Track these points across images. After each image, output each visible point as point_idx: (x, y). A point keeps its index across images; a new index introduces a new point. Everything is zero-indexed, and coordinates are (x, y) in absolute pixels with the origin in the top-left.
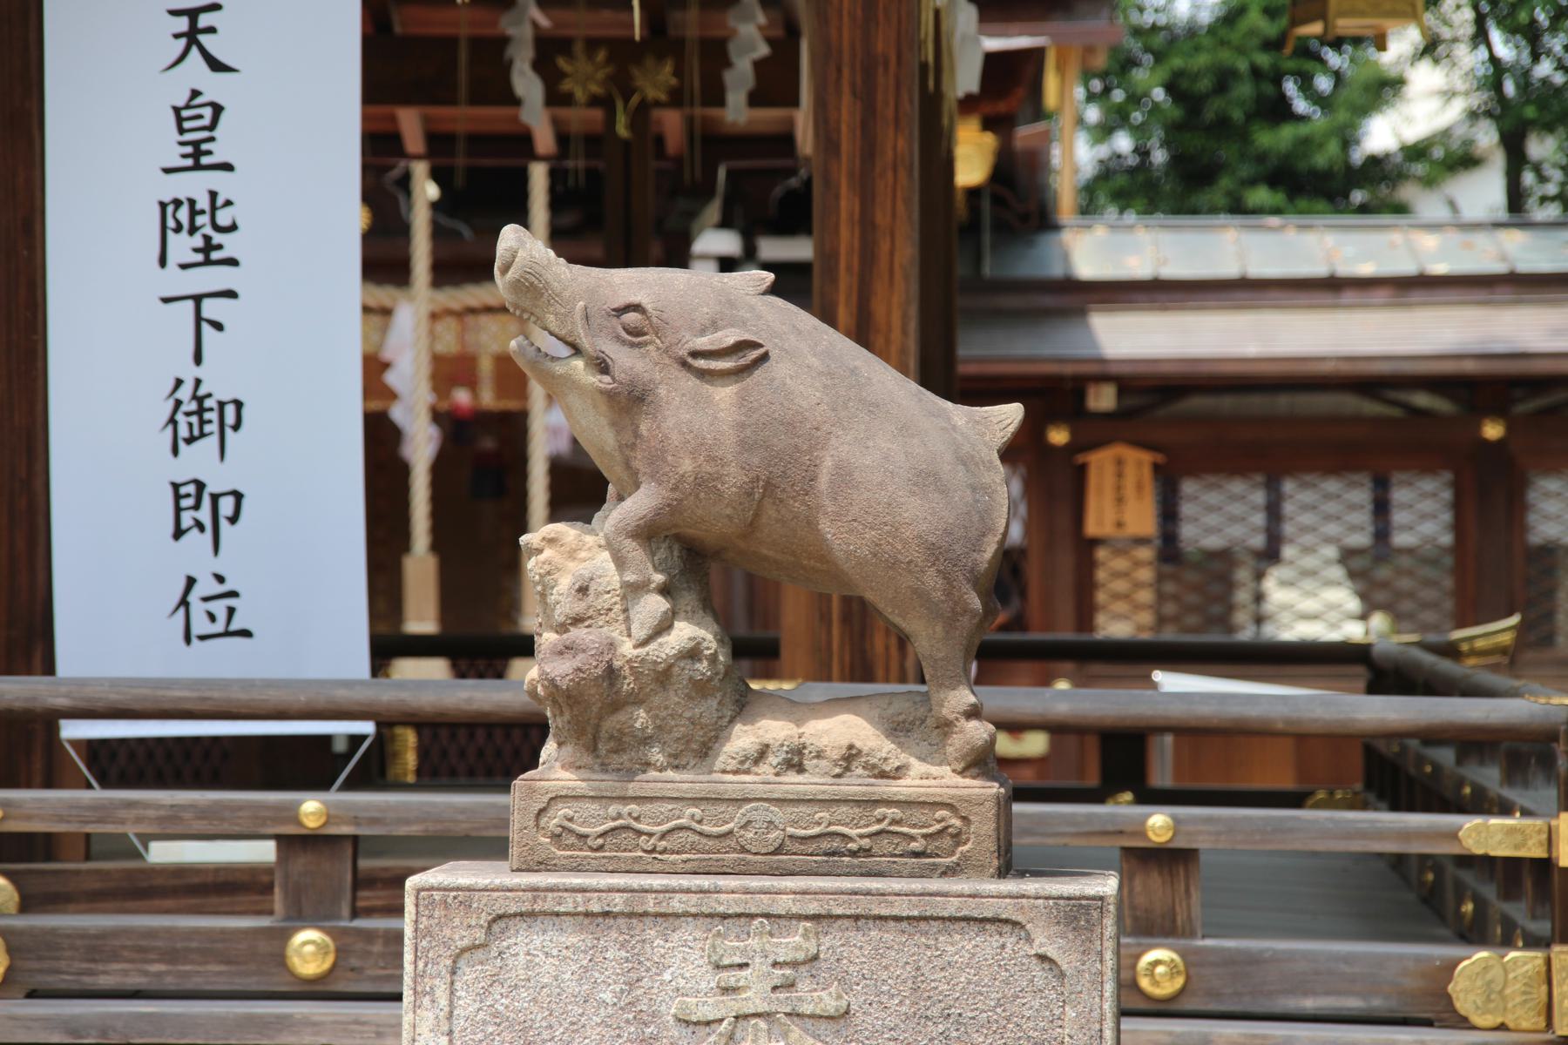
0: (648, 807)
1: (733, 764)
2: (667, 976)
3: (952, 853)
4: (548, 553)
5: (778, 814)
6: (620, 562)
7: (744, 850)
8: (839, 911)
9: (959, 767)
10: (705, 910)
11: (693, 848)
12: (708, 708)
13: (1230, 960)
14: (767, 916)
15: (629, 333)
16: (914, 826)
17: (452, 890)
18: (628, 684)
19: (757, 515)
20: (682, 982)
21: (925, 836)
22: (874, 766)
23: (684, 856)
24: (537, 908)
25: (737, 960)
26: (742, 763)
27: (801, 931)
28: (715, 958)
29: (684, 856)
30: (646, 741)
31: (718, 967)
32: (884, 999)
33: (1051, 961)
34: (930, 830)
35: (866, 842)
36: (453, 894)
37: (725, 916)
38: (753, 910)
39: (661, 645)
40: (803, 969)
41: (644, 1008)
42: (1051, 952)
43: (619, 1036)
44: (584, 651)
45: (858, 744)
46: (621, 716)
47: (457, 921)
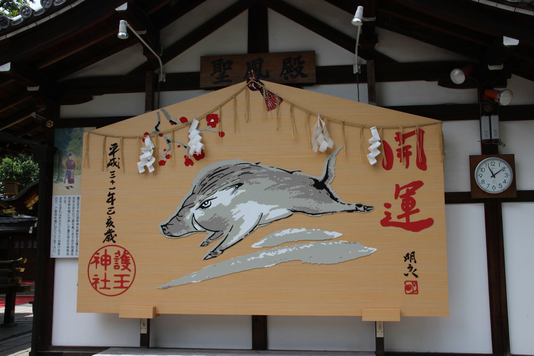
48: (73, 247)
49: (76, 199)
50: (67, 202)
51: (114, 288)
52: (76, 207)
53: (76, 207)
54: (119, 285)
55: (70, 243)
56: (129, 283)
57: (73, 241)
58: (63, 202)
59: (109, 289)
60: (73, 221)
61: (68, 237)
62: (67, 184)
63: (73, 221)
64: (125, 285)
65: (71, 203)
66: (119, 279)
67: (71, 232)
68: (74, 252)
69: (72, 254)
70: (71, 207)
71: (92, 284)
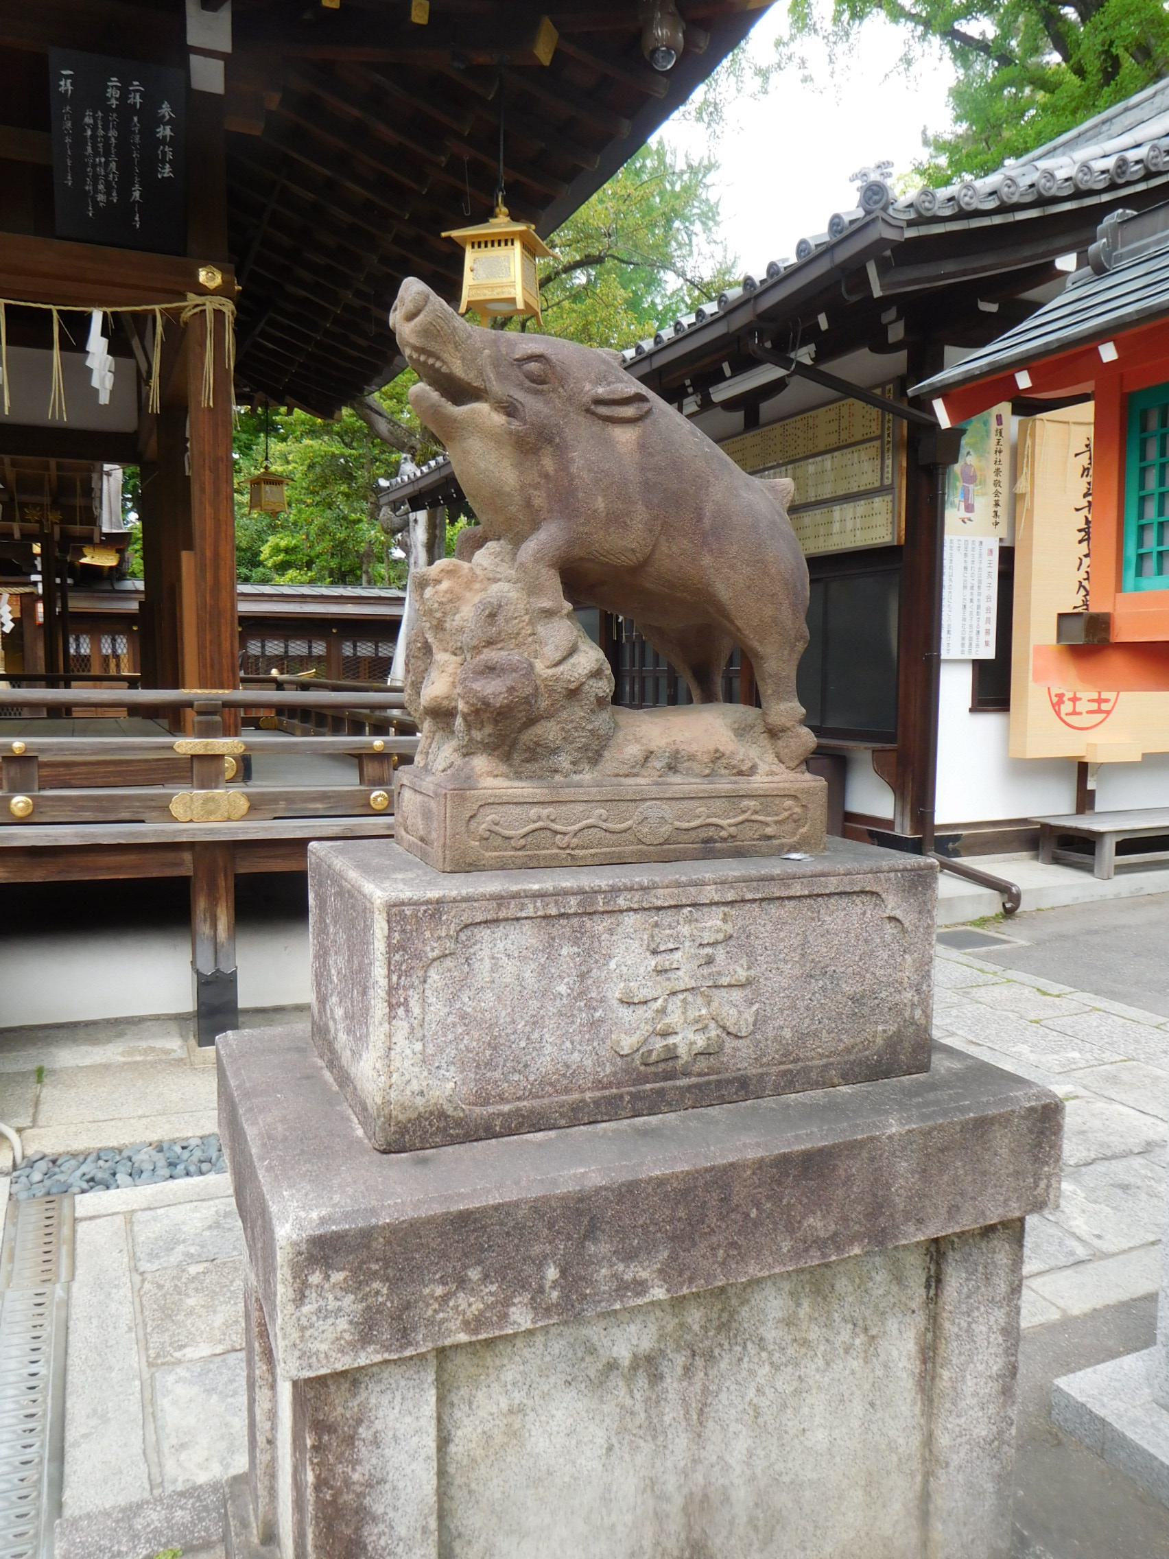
0: (563, 808)
1: (625, 769)
2: (612, 965)
3: (794, 834)
5: (667, 810)
6: (533, 590)
7: (640, 842)
8: (749, 896)
9: (793, 765)
10: (646, 905)
11: (600, 844)
12: (602, 720)
14: (693, 905)
15: (533, 381)
16: (768, 815)
17: (422, 904)
18: (544, 703)
19: (653, 552)
20: (624, 969)
21: (776, 822)
22: (734, 767)
23: (592, 851)
24: (502, 915)
25: (671, 946)
26: (633, 767)
27: (721, 916)
28: (653, 946)
29: (592, 851)
30: (555, 751)
31: (655, 952)
32: (781, 965)
33: (898, 920)
34: (780, 818)
35: (733, 830)
36: (424, 908)
37: (659, 909)
38: (684, 901)
39: (573, 665)
40: (719, 947)
41: (594, 995)
42: (898, 913)
43: (573, 1022)
44: (515, 671)
45: (721, 749)
46: (538, 729)
47: (428, 934)
48: (971, 639)
49: (977, 544)
50: (962, 548)
51: (1088, 712)
52: (977, 560)
53: (977, 560)
54: (1094, 706)
55: (968, 629)
56: (1111, 704)
57: (971, 626)
58: (955, 548)
59: (1080, 714)
60: (972, 588)
61: (964, 619)
62: (963, 513)
63: (972, 588)
64: (1105, 707)
65: (970, 553)
67: (968, 609)
68: (974, 649)
69: (970, 652)
70: (969, 559)
71: (1053, 706)
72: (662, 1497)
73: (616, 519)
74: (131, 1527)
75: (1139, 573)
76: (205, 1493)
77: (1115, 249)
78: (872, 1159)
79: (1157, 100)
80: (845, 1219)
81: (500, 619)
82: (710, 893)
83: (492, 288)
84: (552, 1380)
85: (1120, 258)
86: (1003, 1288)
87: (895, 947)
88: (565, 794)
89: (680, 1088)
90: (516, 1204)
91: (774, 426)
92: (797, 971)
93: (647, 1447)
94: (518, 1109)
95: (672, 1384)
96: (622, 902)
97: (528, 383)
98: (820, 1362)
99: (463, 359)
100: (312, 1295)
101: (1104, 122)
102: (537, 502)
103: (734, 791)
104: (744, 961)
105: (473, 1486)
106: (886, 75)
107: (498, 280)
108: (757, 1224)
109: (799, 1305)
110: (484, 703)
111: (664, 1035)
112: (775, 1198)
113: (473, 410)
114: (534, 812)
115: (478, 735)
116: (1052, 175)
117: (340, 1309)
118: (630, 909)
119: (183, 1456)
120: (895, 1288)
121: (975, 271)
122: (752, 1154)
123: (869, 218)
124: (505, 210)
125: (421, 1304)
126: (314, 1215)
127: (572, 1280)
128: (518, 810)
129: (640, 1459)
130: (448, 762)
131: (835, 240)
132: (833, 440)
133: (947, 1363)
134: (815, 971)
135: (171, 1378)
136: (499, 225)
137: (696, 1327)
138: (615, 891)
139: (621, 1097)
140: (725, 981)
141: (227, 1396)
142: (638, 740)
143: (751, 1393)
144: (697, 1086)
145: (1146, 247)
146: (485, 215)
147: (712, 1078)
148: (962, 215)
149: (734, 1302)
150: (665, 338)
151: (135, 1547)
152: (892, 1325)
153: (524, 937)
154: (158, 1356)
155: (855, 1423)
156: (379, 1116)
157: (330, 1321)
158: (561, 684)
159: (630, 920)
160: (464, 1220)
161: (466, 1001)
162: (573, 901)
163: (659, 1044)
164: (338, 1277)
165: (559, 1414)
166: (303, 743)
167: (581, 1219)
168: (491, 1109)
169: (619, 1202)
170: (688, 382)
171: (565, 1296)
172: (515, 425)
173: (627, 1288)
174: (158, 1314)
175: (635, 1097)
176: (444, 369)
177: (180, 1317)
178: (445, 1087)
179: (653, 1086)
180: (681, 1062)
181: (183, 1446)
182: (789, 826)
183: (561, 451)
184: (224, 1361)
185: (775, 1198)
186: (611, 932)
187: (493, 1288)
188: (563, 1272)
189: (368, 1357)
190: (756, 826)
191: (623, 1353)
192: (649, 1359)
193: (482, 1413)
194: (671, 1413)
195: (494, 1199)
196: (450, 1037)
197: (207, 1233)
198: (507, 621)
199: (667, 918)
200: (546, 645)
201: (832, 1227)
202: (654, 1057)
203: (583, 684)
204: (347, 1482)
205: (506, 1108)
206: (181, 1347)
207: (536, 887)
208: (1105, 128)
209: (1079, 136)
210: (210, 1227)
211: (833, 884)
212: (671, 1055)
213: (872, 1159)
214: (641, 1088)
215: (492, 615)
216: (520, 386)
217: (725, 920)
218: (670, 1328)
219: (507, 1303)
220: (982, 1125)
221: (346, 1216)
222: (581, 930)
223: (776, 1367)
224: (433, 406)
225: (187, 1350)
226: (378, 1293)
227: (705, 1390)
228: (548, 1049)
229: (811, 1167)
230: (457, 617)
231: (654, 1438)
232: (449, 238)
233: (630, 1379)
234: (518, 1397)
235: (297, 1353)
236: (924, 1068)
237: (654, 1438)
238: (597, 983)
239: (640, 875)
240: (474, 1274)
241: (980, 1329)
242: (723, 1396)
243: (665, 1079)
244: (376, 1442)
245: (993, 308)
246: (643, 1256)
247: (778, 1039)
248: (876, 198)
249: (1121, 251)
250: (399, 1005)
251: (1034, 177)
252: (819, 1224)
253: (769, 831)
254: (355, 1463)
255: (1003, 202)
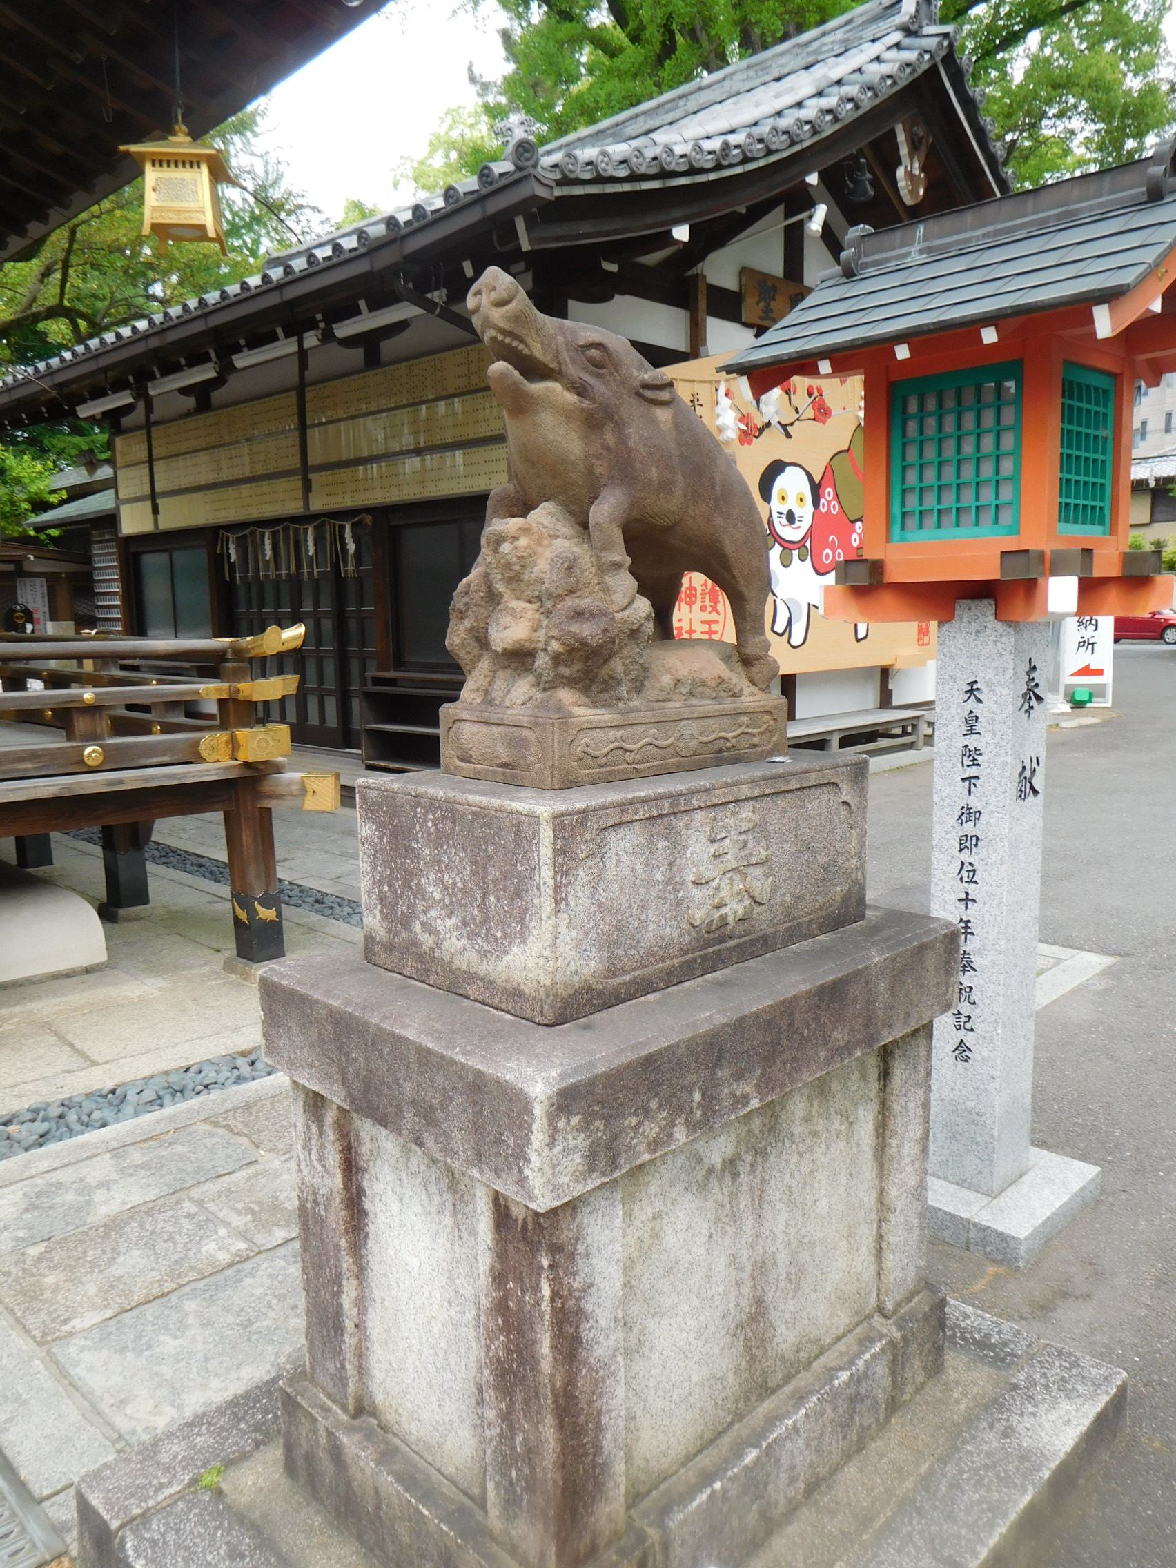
1: (663, 695)
4: (523, 542)
8: (767, 792)
10: (709, 803)
13: (118, 747)
21: (761, 733)
23: (649, 764)
29: (649, 764)
31: (713, 841)
37: (715, 806)
47: (579, 839)
66: (706, 628)
72: (740, 1269)
73: (665, 487)
74: (158, 1463)
75: (903, 528)
76: (213, 1418)
77: (860, 258)
78: (867, 983)
79: (727, 83)
80: (853, 1031)
81: (577, 571)
82: (746, 791)
83: (179, 212)
84: (677, 1188)
85: (865, 266)
86: (923, 1074)
87: (846, 825)
88: (632, 718)
89: (728, 949)
90: (678, 1045)
91: (398, 366)
92: (793, 849)
93: (731, 1230)
94: (635, 978)
95: (744, 1179)
96: (695, 803)
97: (591, 368)
98: (823, 1147)
99: (542, 343)
100: (559, 1137)
101: (681, 97)
102: (598, 470)
103: (735, 709)
104: (764, 843)
105: (633, 1282)
106: (454, 12)
107: (184, 205)
108: (807, 1040)
109: (812, 1105)
110: (581, 644)
111: (717, 907)
112: (816, 1019)
113: (548, 389)
114: (612, 733)
115: (566, 671)
116: (671, 150)
117: (576, 1147)
118: (700, 808)
119: (129, 1410)
120: (862, 1084)
121: (598, 235)
122: (805, 987)
123: (519, 175)
124: (184, 128)
125: (623, 1135)
126: (554, 1073)
127: (709, 1100)
128: (600, 733)
129: (727, 1241)
130: (527, 696)
131: (485, 191)
132: (462, 384)
133: (894, 1133)
134: (804, 848)
135: (72, 1350)
136: (180, 145)
137: (757, 1132)
138: (691, 793)
139: (695, 960)
140: (754, 860)
141: (142, 1351)
142: (668, 671)
143: (787, 1177)
144: (739, 946)
145: (887, 260)
146: (166, 130)
147: (747, 938)
148: (600, 179)
149: (778, 1108)
150: (296, 269)
151: (174, 1476)
152: (861, 1112)
153: (632, 838)
154: (44, 1335)
155: (843, 1189)
156: (547, 997)
157: (570, 1158)
158: (627, 625)
159: (699, 816)
160: (649, 1063)
161: (602, 895)
162: (666, 803)
163: (716, 915)
164: (575, 1120)
165: (681, 1215)
166: (107, 693)
167: (713, 1050)
168: (618, 980)
169: (735, 1034)
170: (319, 317)
171: (704, 1114)
172: (586, 404)
173: (738, 1102)
174: (20, 1298)
175: (704, 958)
176: (526, 351)
177: (48, 1295)
178: (584, 965)
179: (716, 949)
180: (729, 927)
181: (122, 1403)
182: (765, 737)
183: (619, 427)
184: (119, 1322)
185: (816, 1019)
186: (687, 827)
187: (664, 1114)
188: (703, 1095)
189: (594, 1182)
190: (747, 737)
191: (716, 1159)
192: (732, 1161)
193: (637, 1222)
194: (744, 1201)
195: (664, 1043)
196: (592, 924)
197: (27, 1216)
198: (582, 573)
199: (719, 813)
200: (615, 592)
201: (846, 1038)
202: (714, 926)
203: (642, 625)
204: (571, 1291)
205: (627, 978)
206: (66, 1322)
207: (643, 794)
208: (681, 103)
209: (659, 107)
210: (26, 1210)
211: (813, 779)
212: (723, 920)
213: (867, 983)
214: (706, 951)
215: (569, 568)
216: (585, 369)
217: (753, 812)
218: (743, 1134)
219: (672, 1124)
220: (922, 948)
221: (576, 1070)
222: (669, 827)
223: (800, 1155)
224: (514, 383)
225: (73, 1323)
226: (598, 1129)
227: (763, 1181)
228: (652, 926)
229: (832, 995)
230: (535, 570)
231: (735, 1222)
232: (127, 153)
233: (721, 1180)
234: (658, 1205)
235: (551, 1188)
236: (862, 917)
237: (735, 1222)
238: (680, 870)
239: (703, 779)
240: (654, 1105)
241: (911, 1105)
242: (772, 1182)
243: (721, 942)
244: (587, 1255)
245: (614, 268)
246: (747, 1075)
247: (783, 903)
248: (527, 155)
249: (864, 260)
250: (562, 900)
251: (657, 151)
252: (839, 1036)
253: (755, 740)
254: (575, 1273)
255: (632, 171)
